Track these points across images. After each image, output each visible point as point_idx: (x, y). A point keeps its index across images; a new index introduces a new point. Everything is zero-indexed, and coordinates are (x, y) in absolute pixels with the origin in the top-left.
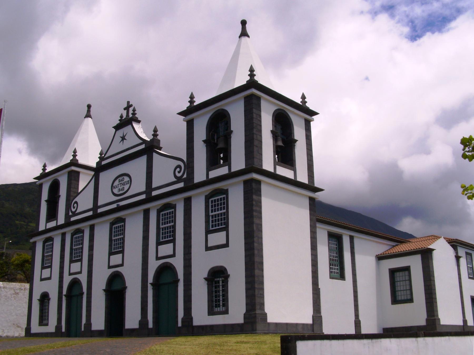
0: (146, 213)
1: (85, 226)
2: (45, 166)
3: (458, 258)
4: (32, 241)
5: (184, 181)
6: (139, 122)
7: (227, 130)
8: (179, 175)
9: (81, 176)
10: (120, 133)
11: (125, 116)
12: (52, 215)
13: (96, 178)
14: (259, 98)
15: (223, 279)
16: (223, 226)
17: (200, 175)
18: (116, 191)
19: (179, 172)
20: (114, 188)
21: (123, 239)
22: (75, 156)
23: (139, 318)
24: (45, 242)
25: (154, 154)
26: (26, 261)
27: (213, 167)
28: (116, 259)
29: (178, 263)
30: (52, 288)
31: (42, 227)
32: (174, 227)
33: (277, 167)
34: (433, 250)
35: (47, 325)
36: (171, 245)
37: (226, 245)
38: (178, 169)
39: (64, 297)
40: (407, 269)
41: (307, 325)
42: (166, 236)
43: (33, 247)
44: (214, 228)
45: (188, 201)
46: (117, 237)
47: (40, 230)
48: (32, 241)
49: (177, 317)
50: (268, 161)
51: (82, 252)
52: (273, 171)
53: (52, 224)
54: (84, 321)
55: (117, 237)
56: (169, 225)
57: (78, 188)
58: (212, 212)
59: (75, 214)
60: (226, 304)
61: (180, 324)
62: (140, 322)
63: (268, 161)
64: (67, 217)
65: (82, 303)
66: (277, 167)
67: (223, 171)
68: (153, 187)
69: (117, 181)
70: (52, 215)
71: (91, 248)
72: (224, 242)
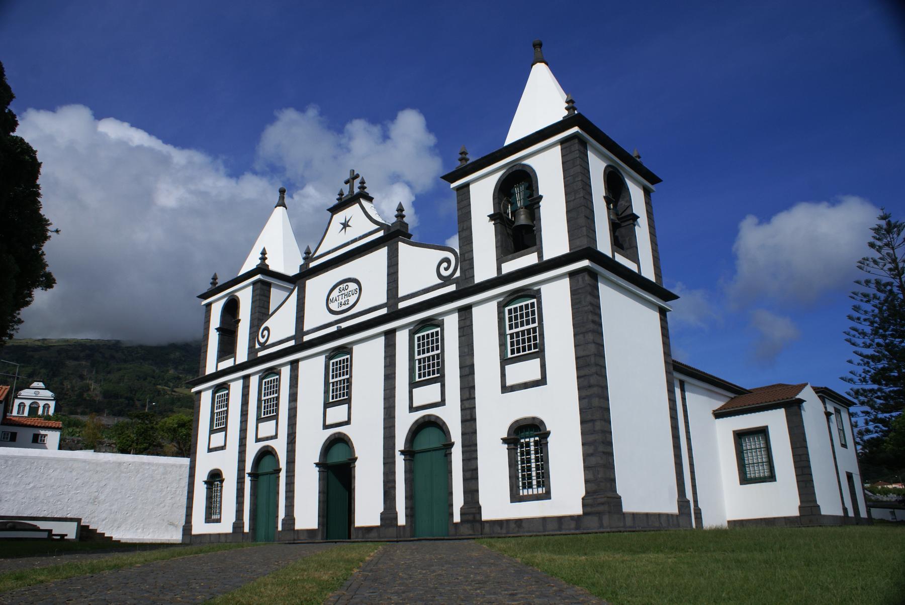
0: (390, 335)
3: (828, 414)
4: (194, 390)
5: (457, 281)
6: (370, 199)
7: (531, 196)
8: (445, 273)
10: (339, 217)
12: (227, 348)
15: (537, 438)
16: (436, 375)
17: (485, 267)
18: (334, 306)
19: (446, 269)
20: (332, 301)
21: (349, 381)
22: (263, 258)
26: (182, 425)
27: (510, 256)
28: (337, 414)
29: (451, 416)
30: (227, 462)
31: (210, 369)
32: (278, 398)
35: (218, 521)
36: (345, 407)
37: (542, 381)
38: (445, 265)
39: (246, 475)
40: (762, 432)
41: (672, 515)
42: (429, 371)
43: (193, 403)
44: (423, 379)
45: (465, 313)
46: (269, 397)
47: (207, 373)
48: (194, 390)
49: (451, 505)
51: (277, 405)
53: (228, 363)
54: (282, 514)
55: (269, 397)
56: (272, 396)
57: (268, 309)
58: (419, 354)
59: (264, 346)
60: (544, 479)
61: (457, 518)
62: (383, 517)
64: (252, 350)
67: (530, 259)
68: (400, 295)
69: (337, 289)
70: (227, 348)
71: (293, 397)
72: (538, 376)
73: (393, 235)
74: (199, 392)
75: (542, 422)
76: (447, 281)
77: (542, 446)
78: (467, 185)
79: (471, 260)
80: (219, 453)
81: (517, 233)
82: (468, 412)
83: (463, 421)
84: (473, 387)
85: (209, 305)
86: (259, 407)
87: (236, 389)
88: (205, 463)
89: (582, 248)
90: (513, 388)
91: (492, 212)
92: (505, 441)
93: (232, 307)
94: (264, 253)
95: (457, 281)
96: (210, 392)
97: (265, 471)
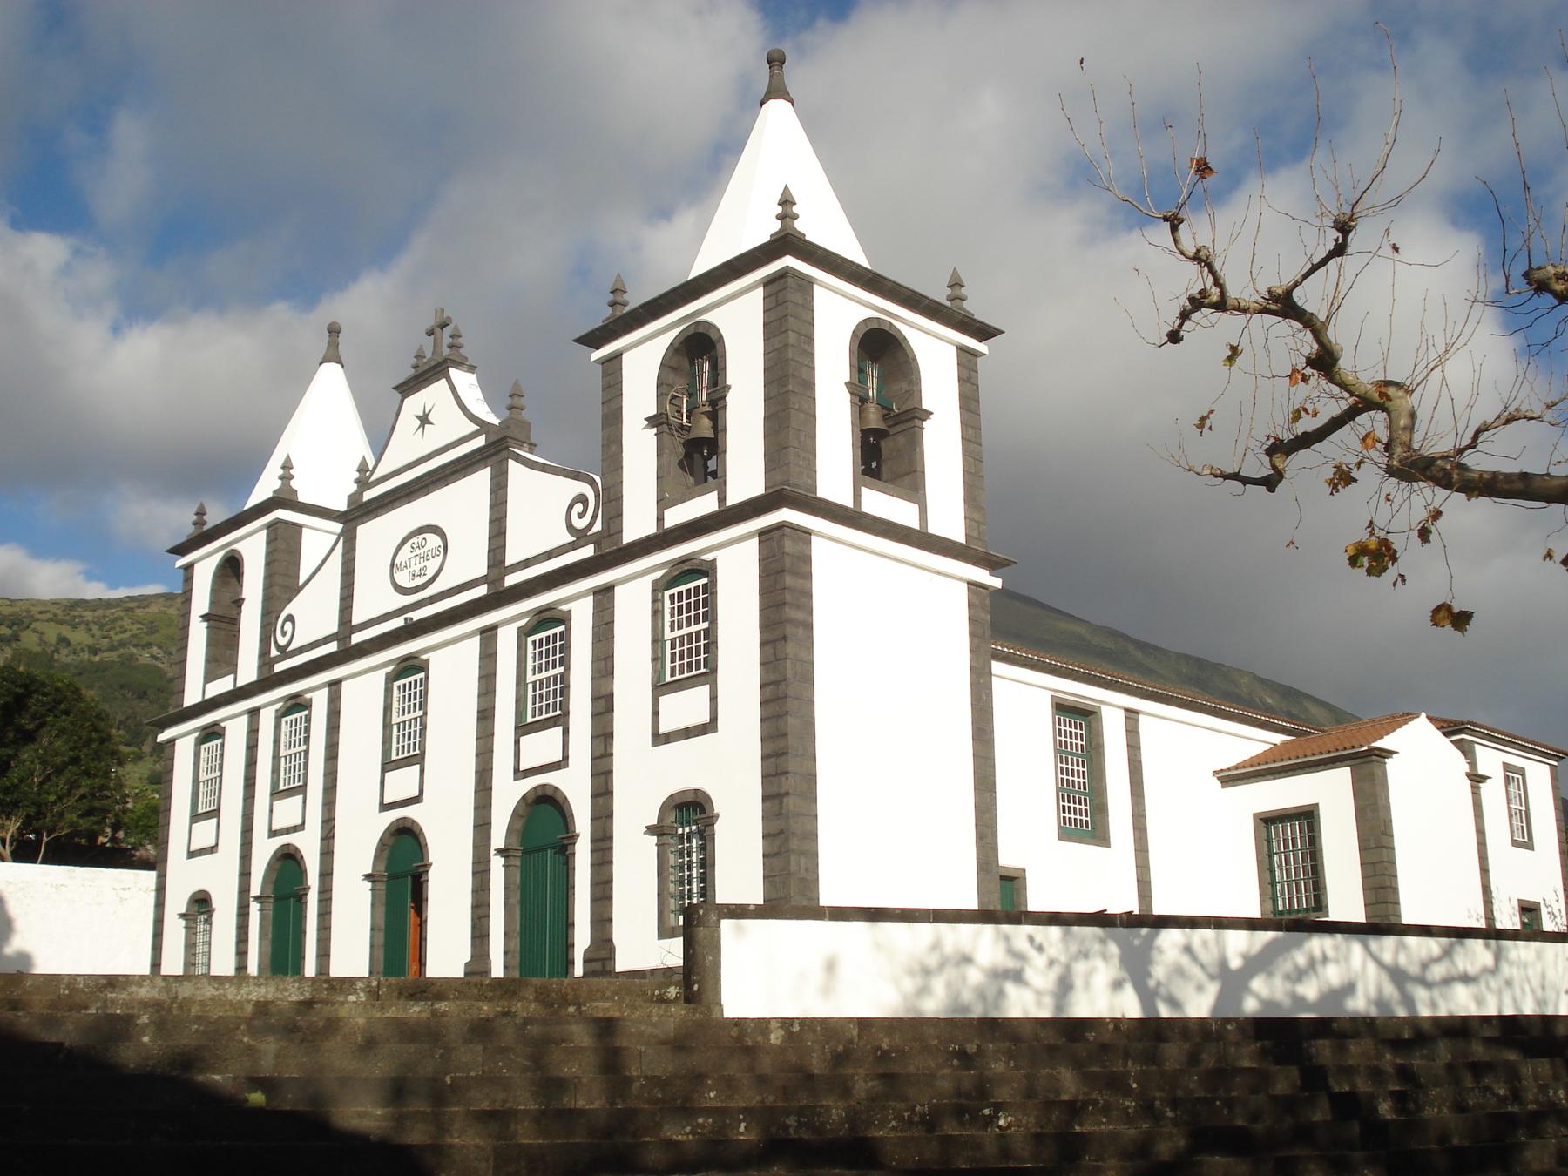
1: (314, 687)
2: (201, 513)
3: (1476, 779)
4: (161, 738)
5: (597, 540)
8: (581, 524)
9: (307, 537)
10: (414, 404)
11: (428, 354)
12: (222, 656)
13: (349, 541)
14: (807, 283)
16: (703, 670)
17: (638, 522)
18: (403, 579)
19: (581, 516)
22: (286, 478)
23: (466, 955)
24: (201, 741)
25: (512, 463)
28: (402, 783)
31: (191, 697)
32: (565, 678)
33: (864, 490)
34: (1390, 753)
37: (709, 727)
38: (579, 507)
40: (1307, 817)
45: (604, 596)
47: (625, 541)
48: (161, 738)
49: (570, 946)
50: (834, 469)
52: (849, 503)
59: (285, 653)
63: (834, 469)
64: (265, 661)
65: (301, 933)
66: (864, 490)
67: (706, 504)
68: (354, 622)
70: (222, 656)
73: (495, 451)
74: (172, 741)
75: (708, 798)
76: (581, 538)
77: (706, 838)
78: (617, 357)
79: (619, 499)
80: (206, 859)
81: (694, 454)
82: (602, 778)
83: (594, 796)
84: (611, 735)
85: (189, 568)
86: (275, 770)
87: (236, 732)
88: (184, 877)
89: (789, 484)
90: (669, 738)
91: (653, 411)
92: (651, 830)
93: (232, 567)
94: (287, 466)
95: (597, 540)
96: (192, 739)
97: (286, 889)
